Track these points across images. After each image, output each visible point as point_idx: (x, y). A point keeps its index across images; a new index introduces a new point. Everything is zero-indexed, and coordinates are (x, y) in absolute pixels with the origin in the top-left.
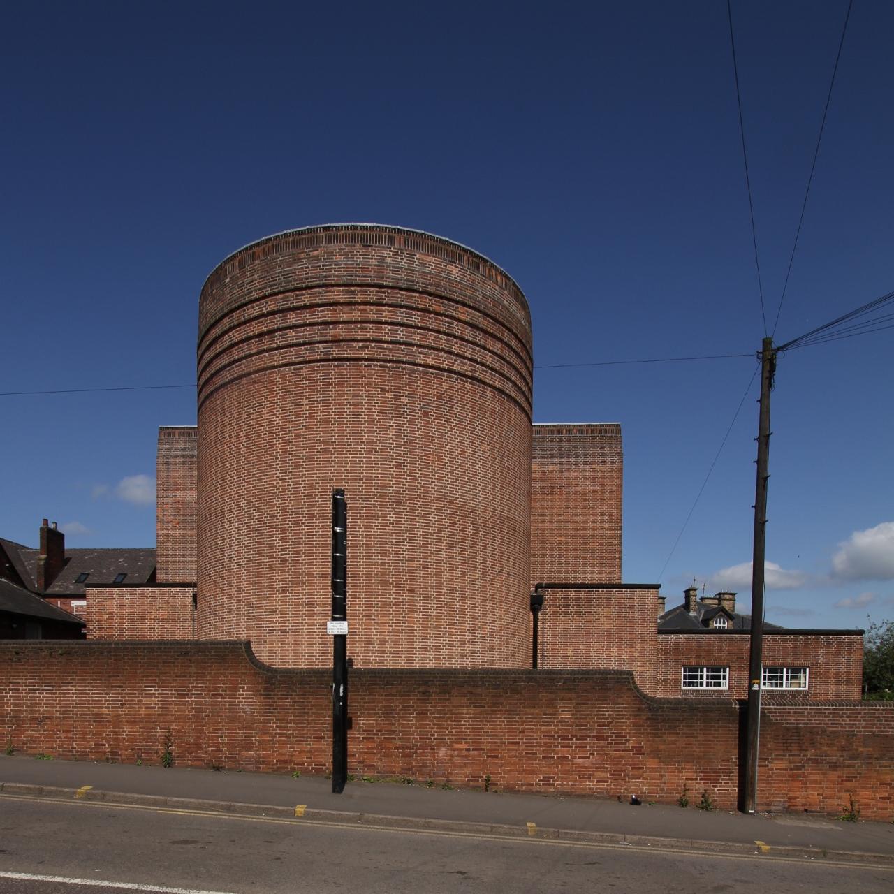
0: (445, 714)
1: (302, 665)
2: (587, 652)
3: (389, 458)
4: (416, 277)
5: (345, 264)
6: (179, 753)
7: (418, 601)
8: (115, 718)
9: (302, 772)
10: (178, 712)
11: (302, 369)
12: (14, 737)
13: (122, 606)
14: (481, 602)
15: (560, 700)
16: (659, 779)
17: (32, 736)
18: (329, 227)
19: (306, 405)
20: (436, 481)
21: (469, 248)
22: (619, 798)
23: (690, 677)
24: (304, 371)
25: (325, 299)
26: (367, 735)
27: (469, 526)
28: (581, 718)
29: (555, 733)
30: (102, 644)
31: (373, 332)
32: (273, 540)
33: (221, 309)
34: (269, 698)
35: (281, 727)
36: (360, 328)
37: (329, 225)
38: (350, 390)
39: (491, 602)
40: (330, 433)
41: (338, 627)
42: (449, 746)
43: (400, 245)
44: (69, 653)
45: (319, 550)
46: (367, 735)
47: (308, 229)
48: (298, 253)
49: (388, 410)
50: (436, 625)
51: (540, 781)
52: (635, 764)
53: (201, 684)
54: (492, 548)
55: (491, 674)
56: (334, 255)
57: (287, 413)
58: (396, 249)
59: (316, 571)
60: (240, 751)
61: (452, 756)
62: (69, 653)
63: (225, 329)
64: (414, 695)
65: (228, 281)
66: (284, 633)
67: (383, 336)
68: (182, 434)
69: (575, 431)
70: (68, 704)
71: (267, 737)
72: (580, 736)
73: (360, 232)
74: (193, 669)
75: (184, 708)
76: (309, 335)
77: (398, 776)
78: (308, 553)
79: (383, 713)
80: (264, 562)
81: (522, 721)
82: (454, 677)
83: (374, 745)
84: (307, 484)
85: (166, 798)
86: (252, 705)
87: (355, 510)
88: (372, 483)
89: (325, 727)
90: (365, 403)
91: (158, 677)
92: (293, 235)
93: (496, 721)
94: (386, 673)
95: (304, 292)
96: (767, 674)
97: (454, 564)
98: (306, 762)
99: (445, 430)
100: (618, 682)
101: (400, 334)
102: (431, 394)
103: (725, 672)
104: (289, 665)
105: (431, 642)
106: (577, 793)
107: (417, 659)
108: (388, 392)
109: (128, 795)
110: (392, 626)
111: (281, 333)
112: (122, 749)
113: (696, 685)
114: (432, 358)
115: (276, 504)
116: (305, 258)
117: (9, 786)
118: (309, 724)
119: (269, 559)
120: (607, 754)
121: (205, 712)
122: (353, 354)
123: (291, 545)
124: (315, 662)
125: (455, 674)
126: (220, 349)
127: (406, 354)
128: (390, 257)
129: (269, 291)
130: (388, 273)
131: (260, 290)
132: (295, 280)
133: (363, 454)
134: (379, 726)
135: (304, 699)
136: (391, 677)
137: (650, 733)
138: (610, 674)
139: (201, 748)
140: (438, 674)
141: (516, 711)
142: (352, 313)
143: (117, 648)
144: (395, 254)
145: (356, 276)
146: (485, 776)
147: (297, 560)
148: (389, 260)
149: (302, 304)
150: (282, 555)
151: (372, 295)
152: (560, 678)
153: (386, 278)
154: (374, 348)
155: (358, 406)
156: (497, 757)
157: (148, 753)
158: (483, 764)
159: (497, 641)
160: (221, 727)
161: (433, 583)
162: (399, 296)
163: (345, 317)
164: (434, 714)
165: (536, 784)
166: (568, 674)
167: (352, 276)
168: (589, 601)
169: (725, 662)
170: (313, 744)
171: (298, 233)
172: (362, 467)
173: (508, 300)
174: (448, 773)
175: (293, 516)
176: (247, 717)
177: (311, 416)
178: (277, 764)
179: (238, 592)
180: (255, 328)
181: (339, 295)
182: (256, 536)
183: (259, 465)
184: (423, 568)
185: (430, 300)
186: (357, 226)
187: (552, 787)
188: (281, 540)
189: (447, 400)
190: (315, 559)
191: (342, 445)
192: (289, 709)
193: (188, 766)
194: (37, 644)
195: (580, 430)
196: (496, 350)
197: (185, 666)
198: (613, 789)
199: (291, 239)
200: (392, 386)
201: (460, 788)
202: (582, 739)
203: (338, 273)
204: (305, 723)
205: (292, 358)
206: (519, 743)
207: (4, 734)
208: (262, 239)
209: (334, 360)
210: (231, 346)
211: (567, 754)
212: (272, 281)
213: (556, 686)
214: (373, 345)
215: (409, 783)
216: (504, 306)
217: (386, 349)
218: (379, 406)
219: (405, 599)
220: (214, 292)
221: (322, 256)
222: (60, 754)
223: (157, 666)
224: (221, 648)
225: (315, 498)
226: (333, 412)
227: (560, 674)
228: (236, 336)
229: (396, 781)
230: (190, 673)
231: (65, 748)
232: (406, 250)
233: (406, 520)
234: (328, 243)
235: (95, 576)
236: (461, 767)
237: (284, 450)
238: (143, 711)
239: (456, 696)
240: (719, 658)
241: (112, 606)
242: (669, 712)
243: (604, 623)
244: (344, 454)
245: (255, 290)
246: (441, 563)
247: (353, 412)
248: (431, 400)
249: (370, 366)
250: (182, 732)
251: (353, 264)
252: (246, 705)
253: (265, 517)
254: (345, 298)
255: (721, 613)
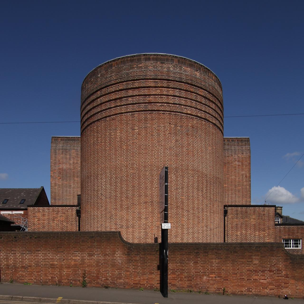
0: (206, 262)
1: (136, 241)
2: (246, 234)
3: (173, 153)
4: (183, 76)
5: (153, 70)
6: (89, 281)
7: (185, 213)
8: (60, 266)
9: (144, 288)
10: (89, 263)
11: (135, 114)
12: (14, 275)
13: (44, 215)
14: (209, 213)
15: (254, 255)
16: (295, 288)
17: (22, 274)
18: (146, 54)
19: (137, 129)
20: (192, 162)
21: (203, 65)
22: (279, 296)
23: (295, 244)
24: (136, 115)
25: (145, 85)
26: (172, 271)
27: (204, 181)
28: (262, 263)
29: (252, 269)
30: (54, 233)
31: (165, 99)
32: (122, 187)
33: (96, 87)
34: (130, 256)
35: (135, 269)
36: (160, 98)
37: (146, 53)
38: (156, 124)
39: (213, 214)
40: (147, 142)
41: (166, 226)
42: (207, 276)
43: (176, 63)
44: (39, 237)
45: (143, 191)
46: (172, 271)
47: (137, 55)
48: (133, 65)
49: (172, 132)
50: (192, 223)
51: (246, 290)
52: (285, 282)
53: (99, 250)
54: (213, 191)
55: (225, 245)
56: (148, 66)
57: (128, 133)
58: (174, 64)
59: (142, 201)
60: (117, 279)
61: (209, 280)
62: (39, 237)
63: (99, 96)
64: (192, 254)
65: (99, 75)
66: (128, 227)
67: (169, 101)
68: (62, 140)
69: (230, 140)
70: (39, 260)
71: (128, 273)
72: (262, 271)
73: (160, 57)
74: (95, 244)
75: (91, 261)
76: (138, 100)
77: (186, 289)
78: (138, 193)
79: (179, 262)
80: (118, 197)
81: (238, 265)
82: (209, 246)
83: (175, 276)
84: (138, 163)
85: (97, 302)
86: (122, 259)
87: (172, 177)
88: (166, 163)
89: (154, 269)
90: (163, 129)
91: (80, 247)
92: (130, 57)
93: (227, 265)
94: (180, 245)
95: (135, 82)
96: (294, 242)
97: (199, 198)
98: (146, 284)
99: (195, 141)
100: (278, 248)
101: (177, 100)
102: (189, 126)
103: (300, 241)
104: (130, 241)
105: (191, 231)
106: (262, 295)
107: (185, 238)
108: (172, 124)
109: (80, 301)
110: (175, 224)
111: (125, 99)
112: (64, 280)
113: (288, 247)
114: (190, 111)
115: (124, 172)
116: (136, 67)
117: (25, 298)
118: (147, 267)
119: (120, 195)
120: (273, 278)
121: (101, 263)
122: (157, 108)
123: (131, 189)
124: (142, 240)
125: (210, 245)
126: (96, 105)
127: (179, 109)
128: (172, 68)
129: (120, 80)
130: (172, 74)
131: (115, 80)
132: (131, 77)
133: (162, 151)
134: (177, 268)
135: (145, 256)
136: (183, 247)
137: (291, 269)
138: (274, 244)
139: (99, 279)
140: (203, 245)
141: (236, 260)
142: (157, 91)
143: (61, 235)
144: (174, 66)
145: (158, 75)
146: (223, 288)
147: (133, 196)
148: (172, 69)
149: (135, 87)
150: (126, 193)
151: (165, 84)
152: (254, 246)
153: (171, 77)
154: (166, 106)
155: (160, 130)
156: (228, 280)
157: (75, 281)
158: (222, 283)
159: (215, 230)
160: (108, 269)
161: (191, 206)
162: (176, 84)
163: (154, 93)
164: (201, 262)
165: (244, 291)
166: (257, 244)
167: (156, 75)
168: (246, 212)
169: (300, 237)
170: (149, 276)
171: (132, 57)
172: (162, 156)
173: (217, 87)
174: (207, 287)
175: (132, 177)
176: (120, 264)
177: (139, 134)
178: (133, 285)
179: (106, 209)
180: (113, 96)
181: (151, 83)
182: (114, 185)
183: (115, 155)
184: (187, 199)
185: (189, 86)
186: (158, 54)
187: (251, 292)
188: (126, 187)
189: (195, 128)
190: (141, 195)
191: (153, 147)
192: (138, 261)
193: (93, 287)
194: (24, 233)
195: (233, 140)
196: (213, 108)
197: (92, 243)
198: (277, 293)
199: (129, 59)
200: (173, 122)
201: (212, 294)
202: (263, 272)
203: (150, 74)
204: (145, 267)
205: (130, 110)
206: (237, 274)
207: (9, 274)
208: (116, 58)
209: (149, 111)
210: (101, 104)
211: (257, 278)
212: (121, 77)
213: (252, 249)
214: (165, 105)
215: (190, 292)
216: (216, 89)
217: (171, 106)
218: (168, 131)
219: (180, 213)
220: (92, 80)
221: (143, 67)
222: (34, 282)
223: (79, 243)
224: (108, 235)
225: (141, 169)
226: (149, 133)
227: (254, 244)
228: (103, 99)
229: (185, 291)
230: (94, 246)
231: (37, 279)
232: (179, 65)
233: (180, 179)
234: (146, 61)
235: (11, 201)
236: (212, 284)
237: (127, 149)
238: (73, 263)
239: (211, 254)
240: (298, 236)
241: (39, 215)
242: (299, 260)
243: (253, 222)
244: (154, 151)
245: (113, 80)
246: (194, 197)
247: (157, 133)
248: (189, 128)
249: (164, 113)
250: (91, 272)
251: (157, 70)
252: (119, 259)
253: (118, 177)
254: (154, 85)
255: (277, 215)
